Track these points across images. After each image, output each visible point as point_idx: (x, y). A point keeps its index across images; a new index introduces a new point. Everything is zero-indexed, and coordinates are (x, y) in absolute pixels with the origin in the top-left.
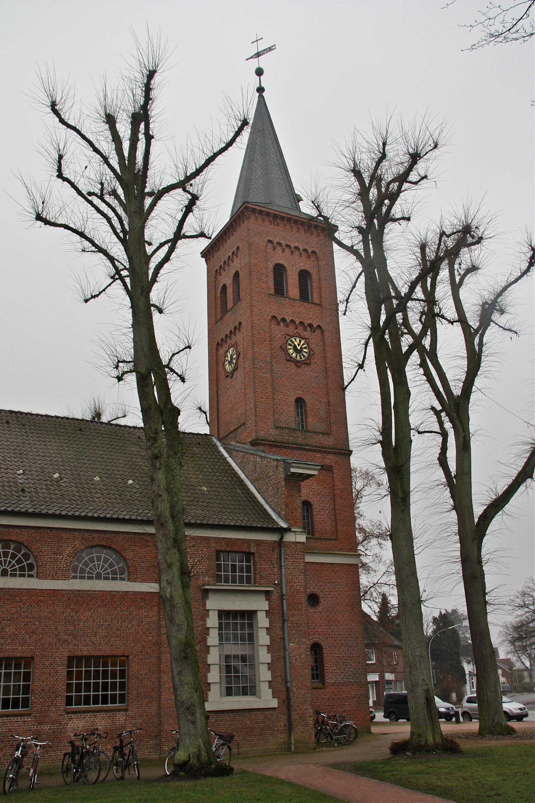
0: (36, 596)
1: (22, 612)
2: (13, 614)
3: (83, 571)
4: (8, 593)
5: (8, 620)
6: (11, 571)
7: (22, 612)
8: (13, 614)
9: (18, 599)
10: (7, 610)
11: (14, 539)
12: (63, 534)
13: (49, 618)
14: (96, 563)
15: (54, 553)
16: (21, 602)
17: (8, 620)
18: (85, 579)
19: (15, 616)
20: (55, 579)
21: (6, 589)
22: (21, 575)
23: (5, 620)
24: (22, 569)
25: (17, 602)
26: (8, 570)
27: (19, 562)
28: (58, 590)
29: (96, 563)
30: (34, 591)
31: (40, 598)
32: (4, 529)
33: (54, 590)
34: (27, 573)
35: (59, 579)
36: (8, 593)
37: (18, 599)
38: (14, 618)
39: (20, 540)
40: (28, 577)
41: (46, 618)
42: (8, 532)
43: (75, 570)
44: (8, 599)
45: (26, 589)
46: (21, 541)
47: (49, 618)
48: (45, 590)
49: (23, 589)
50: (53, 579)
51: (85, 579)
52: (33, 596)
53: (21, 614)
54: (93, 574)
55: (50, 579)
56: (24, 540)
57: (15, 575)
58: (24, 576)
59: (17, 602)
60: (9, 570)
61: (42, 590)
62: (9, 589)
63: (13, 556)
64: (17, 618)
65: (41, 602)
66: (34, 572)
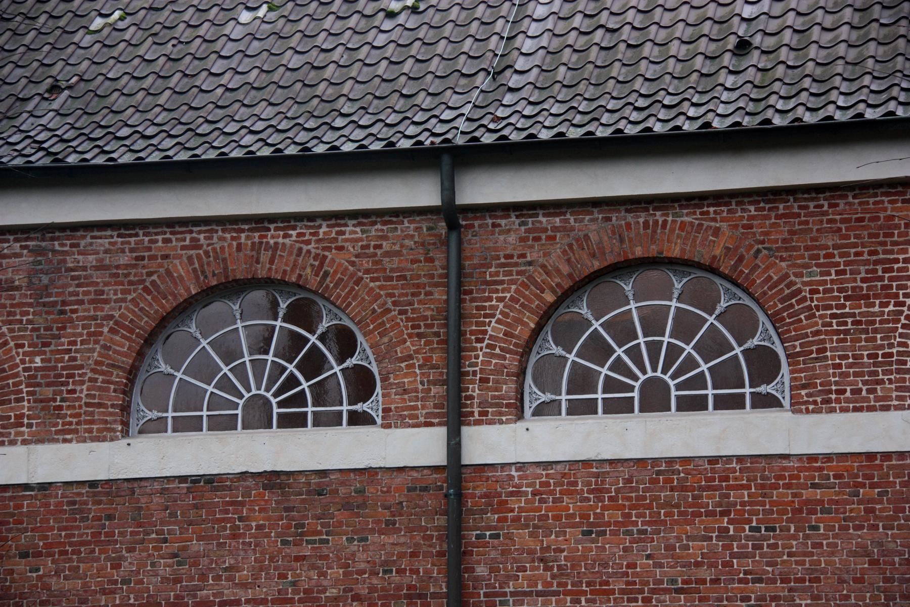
0: (788, 486)
1: (733, 555)
2: (698, 564)
3: (582, 381)
4: (666, 481)
5: (679, 591)
6: (679, 387)
7: (733, 555)
8: (698, 564)
9: (710, 501)
10: (670, 548)
11: (676, 252)
12: (889, 206)
13: (856, 580)
14: (619, 351)
15: (856, 296)
16: (723, 514)
17: (679, 591)
18: (304, 425)
19: (707, 574)
20: (871, 409)
21: (656, 461)
22: (723, 403)
23: (666, 591)
24: (722, 376)
25: (709, 514)
26: (267, 402)
27: (712, 346)
28: (887, 456)
29: (619, 351)
30: (776, 464)
31: (806, 494)
32: (630, 217)
33: (871, 456)
34: (747, 390)
35: (886, 408)
36: (669, 481)
37: (710, 501)
38: (704, 581)
39: (702, 254)
40: (754, 406)
41: (841, 581)
42: (646, 225)
43: (548, 382)
44: (668, 504)
45: (740, 459)
46: (706, 261)
47: (856, 580)
48: (828, 457)
49: (729, 458)
50: (856, 409)
51: (304, 425)
52: (775, 487)
53: (729, 564)
54: (631, 389)
55: (844, 410)
56: (717, 252)
57: (698, 404)
58: (736, 403)
59: (709, 514)
60: (672, 383)
61: (813, 458)
62: (671, 461)
63: (685, 327)
64: (716, 581)
65: (813, 512)
66: (782, 384)
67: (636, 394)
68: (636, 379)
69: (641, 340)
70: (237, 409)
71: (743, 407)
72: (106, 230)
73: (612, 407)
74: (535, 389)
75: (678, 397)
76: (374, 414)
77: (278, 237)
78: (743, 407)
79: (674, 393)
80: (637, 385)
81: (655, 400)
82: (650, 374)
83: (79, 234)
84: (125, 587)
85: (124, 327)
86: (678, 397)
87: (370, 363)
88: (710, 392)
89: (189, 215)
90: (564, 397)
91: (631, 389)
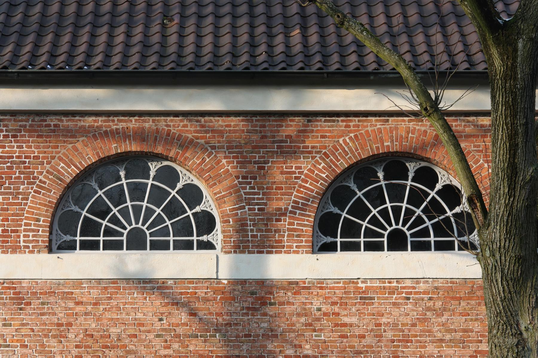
24: (439, 230)
54: (382, 236)
58: (188, 246)
67: (124, 238)
68: (125, 228)
69: (129, 203)
70: (150, 233)
71: (168, 249)
72: (160, 117)
73: (370, 247)
74: (320, 234)
75: (411, 241)
76: (214, 243)
77: (367, 126)
78: (168, 249)
79: (409, 239)
80: (126, 232)
81: (397, 243)
82: (140, 225)
83: (77, 118)
84: (372, 355)
85: (311, 178)
86: (150, 240)
87: (212, 210)
88: (171, 238)
89: (362, 109)
90: (78, 238)
91: (122, 235)
